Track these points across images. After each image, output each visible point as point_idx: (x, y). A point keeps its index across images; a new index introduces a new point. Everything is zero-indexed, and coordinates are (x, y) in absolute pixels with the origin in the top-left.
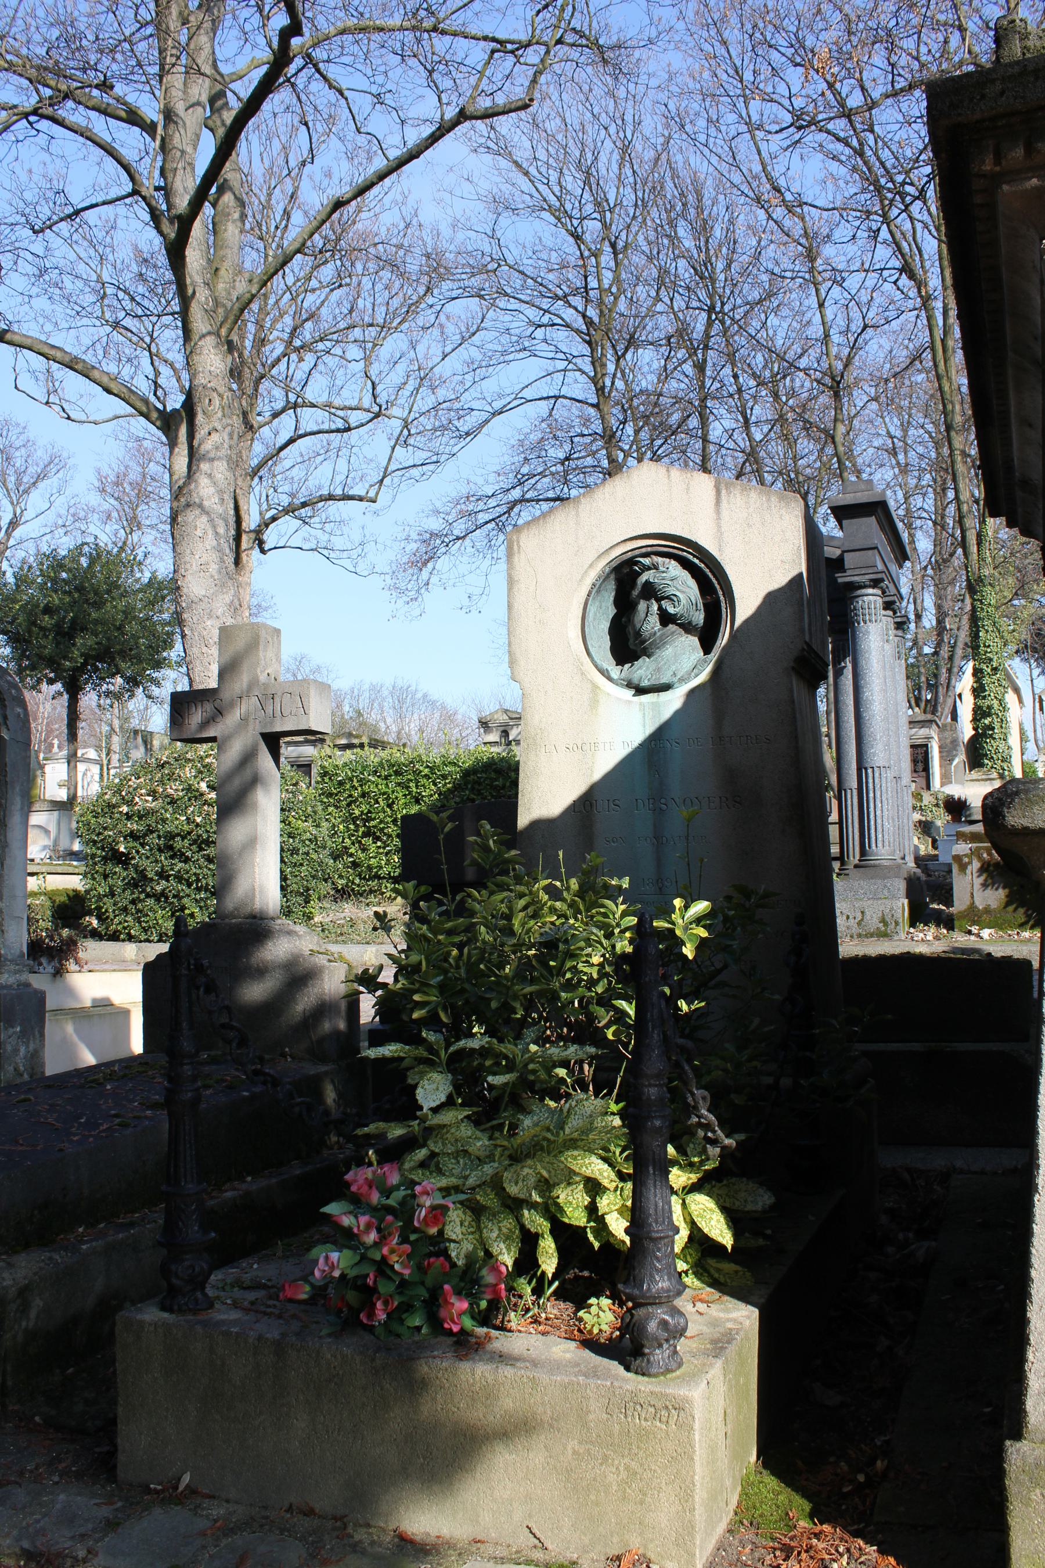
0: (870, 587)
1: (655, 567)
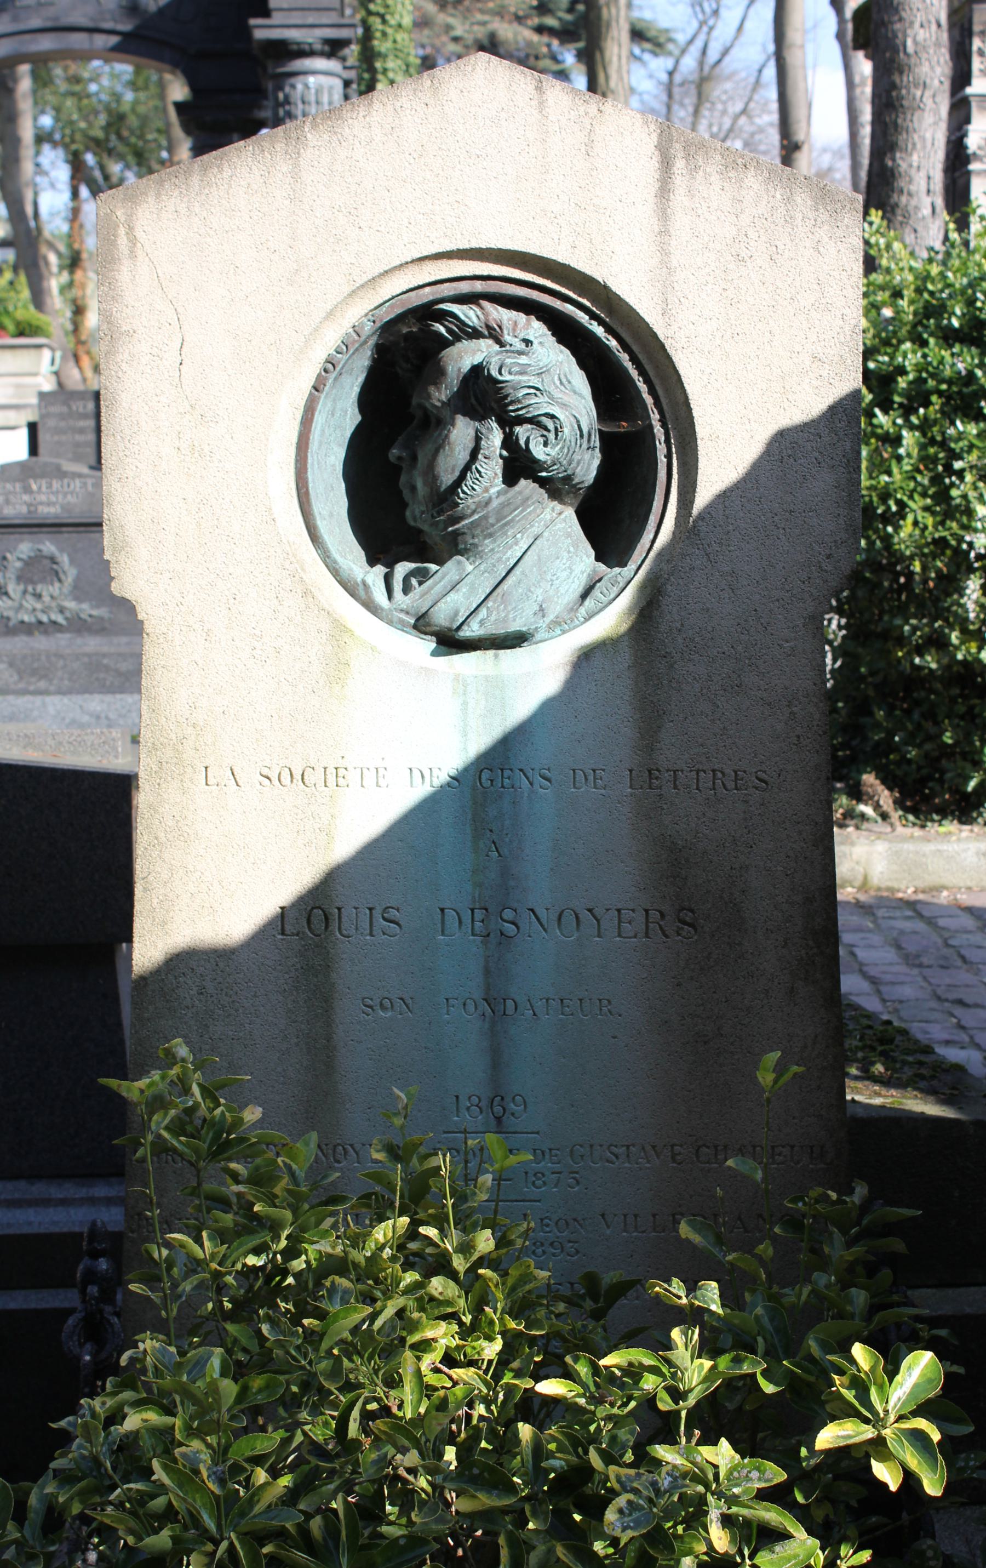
0: (322, 54)
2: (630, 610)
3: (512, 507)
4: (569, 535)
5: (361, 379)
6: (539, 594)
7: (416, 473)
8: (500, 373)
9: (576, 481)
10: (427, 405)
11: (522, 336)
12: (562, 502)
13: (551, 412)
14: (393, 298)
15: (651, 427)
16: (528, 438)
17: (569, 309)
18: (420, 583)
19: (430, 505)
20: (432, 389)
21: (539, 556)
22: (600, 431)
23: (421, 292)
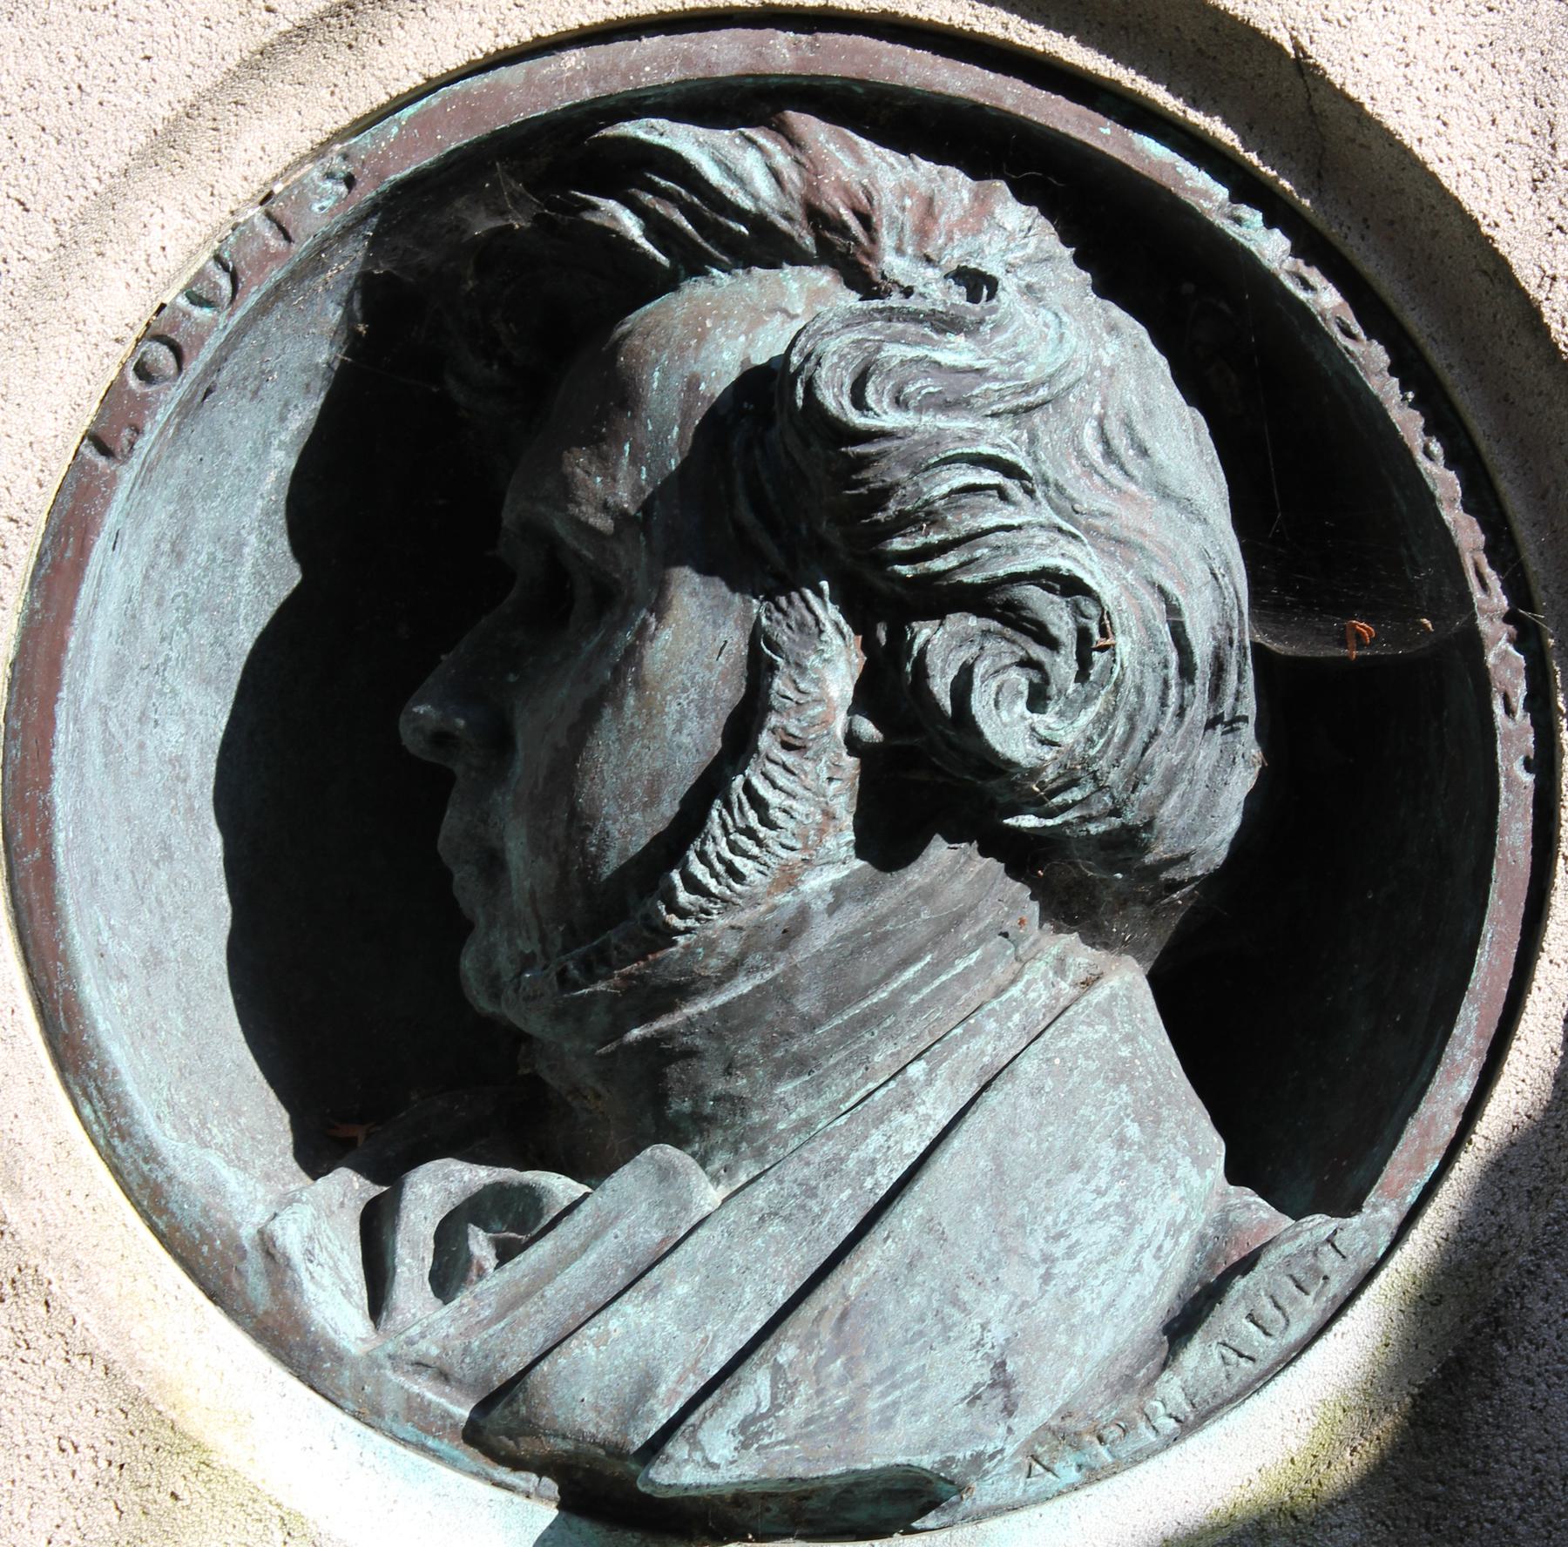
1: (837, 244)
2: (1375, 1392)
3: (893, 951)
4: (1121, 1074)
5: (303, 416)
6: (992, 1314)
7: (503, 800)
8: (859, 402)
9: (1159, 851)
10: (560, 527)
11: (954, 257)
12: (1096, 936)
13: (1066, 565)
14: (432, 86)
15: (1473, 644)
16: (966, 671)
17: (1150, 154)
18: (506, 1252)
19: (557, 935)
20: (579, 463)
21: (997, 1157)
22: (1257, 647)
23: (546, 67)
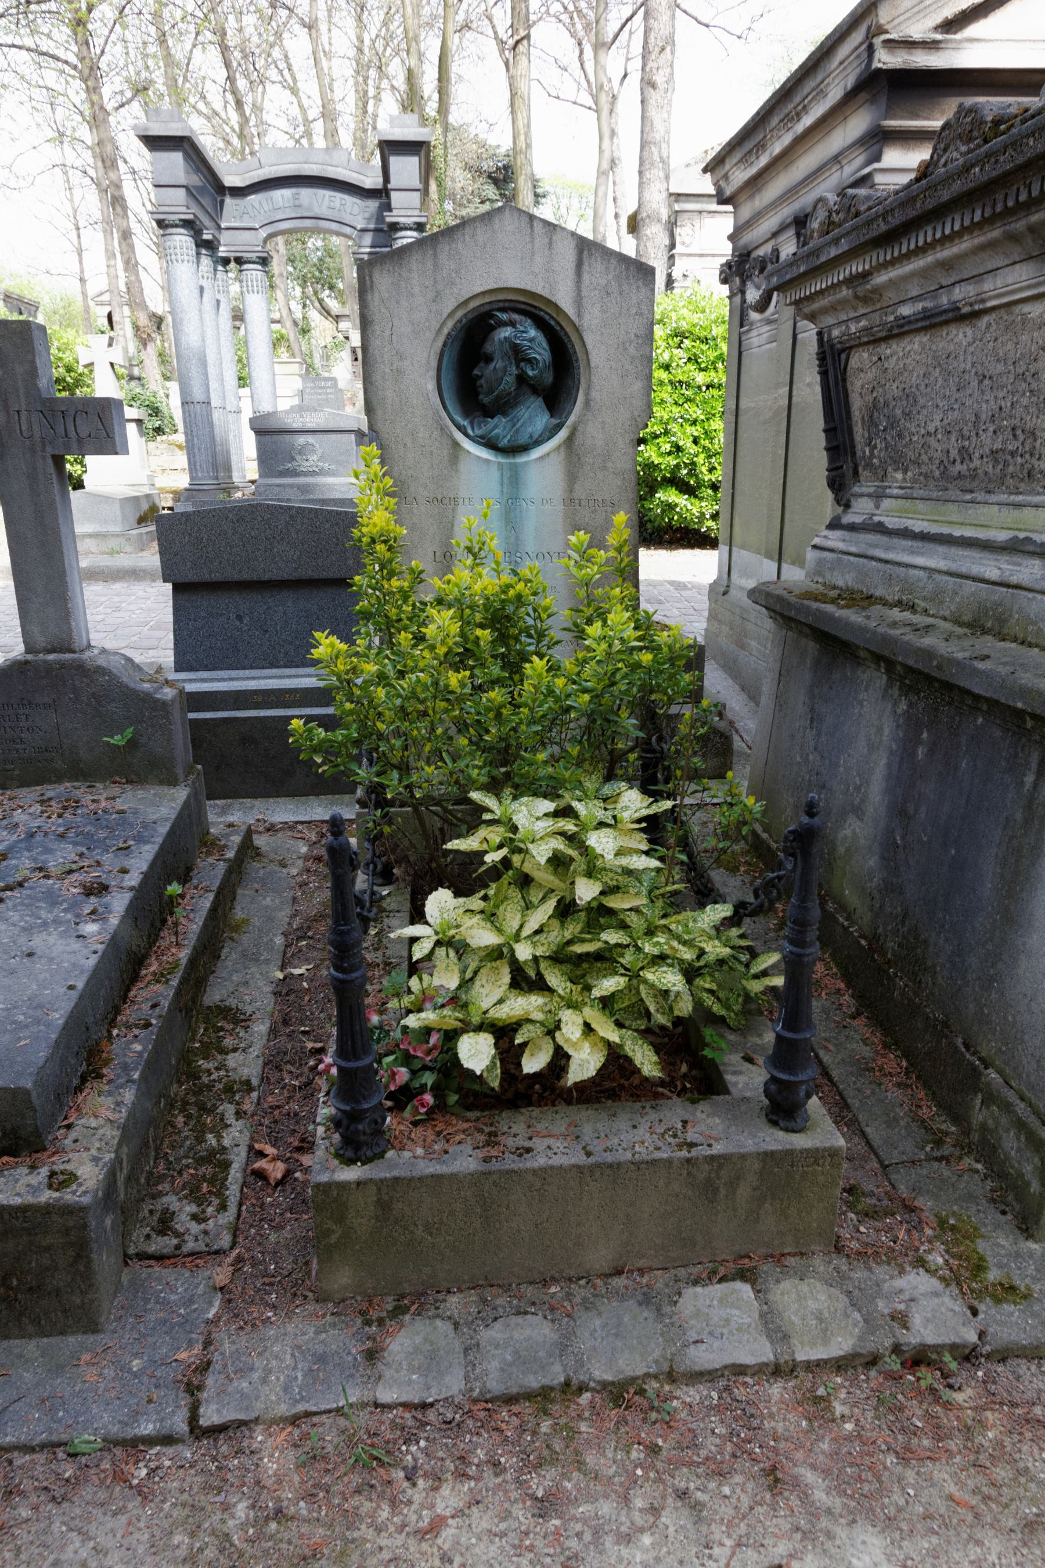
1: (512, 324)
